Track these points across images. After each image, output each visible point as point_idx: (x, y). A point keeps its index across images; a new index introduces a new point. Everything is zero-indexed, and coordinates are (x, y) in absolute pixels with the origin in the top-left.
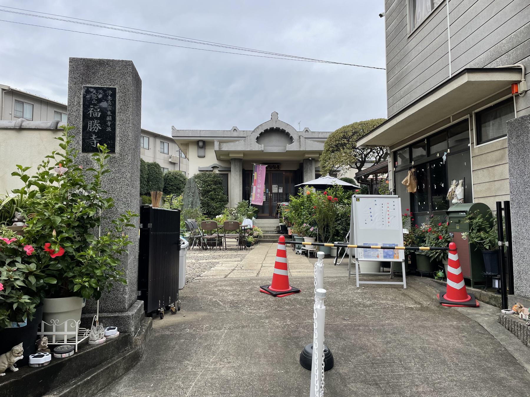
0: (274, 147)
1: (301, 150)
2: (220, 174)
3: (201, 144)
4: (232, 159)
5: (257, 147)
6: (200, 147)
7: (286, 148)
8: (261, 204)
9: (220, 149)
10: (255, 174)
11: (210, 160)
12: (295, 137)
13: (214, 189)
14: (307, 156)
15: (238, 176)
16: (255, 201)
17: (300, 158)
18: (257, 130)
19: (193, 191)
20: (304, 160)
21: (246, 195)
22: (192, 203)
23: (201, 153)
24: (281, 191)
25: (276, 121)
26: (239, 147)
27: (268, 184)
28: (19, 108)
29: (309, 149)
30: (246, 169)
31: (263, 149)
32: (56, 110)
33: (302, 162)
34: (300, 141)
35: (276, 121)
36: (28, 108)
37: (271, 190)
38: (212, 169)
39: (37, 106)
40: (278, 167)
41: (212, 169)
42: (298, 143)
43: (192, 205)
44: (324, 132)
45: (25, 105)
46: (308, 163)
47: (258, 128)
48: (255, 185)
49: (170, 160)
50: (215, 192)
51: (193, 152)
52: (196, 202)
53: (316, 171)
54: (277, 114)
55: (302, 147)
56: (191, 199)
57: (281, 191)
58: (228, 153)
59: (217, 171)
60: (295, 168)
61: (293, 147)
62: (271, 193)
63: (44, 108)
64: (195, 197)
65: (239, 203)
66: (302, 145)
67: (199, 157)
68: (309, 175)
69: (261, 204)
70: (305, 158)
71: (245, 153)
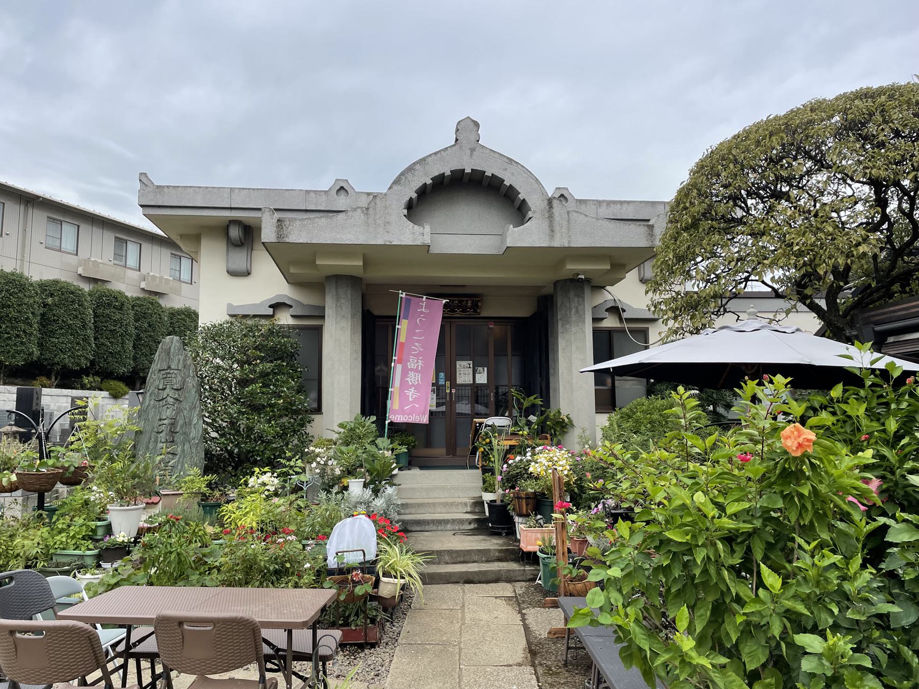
0: (466, 236)
1: (556, 244)
2: (294, 327)
3: (235, 232)
4: (328, 278)
5: (406, 234)
6: (235, 245)
7: (503, 241)
8: (425, 420)
9: (279, 236)
10: (403, 327)
11: (266, 286)
12: (535, 203)
13: (264, 375)
14: (572, 267)
15: (348, 332)
16: (403, 412)
17: (541, 278)
18: (409, 176)
19: (177, 381)
20: (556, 283)
21: (374, 395)
22: (173, 425)
23: (239, 259)
24: (482, 378)
25: (472, 150)
26: (350, 232)
27: (445, 362)
28: (53, 229)
29: (581, 241)
30: (376, 312)
31: (427, 240)
32: (50, 215)
33: (549, 290)
34: (551, 217)
35: (472, 150)
36: (69, 231)
37: (451, 376)
38: (270, 311)
39: (85, 228)
40: (475, 307)
41: (270, 311)
42: (545, 225)
43: (173, 433)
44: (615, 202)
45: (130, 245)
46: (572, 294)
47: (411, 169)
48: (400, 361)
49: (143, 285)
50: (265, 385)
51: (213, 261)
52: (187, 424)
53: (595, 320)
54: (477, 125)
55: (558, 235)
56: (168, 413)
57: (482, 378)
58: (314, 251)
59: (285, 319)
60: (523, 311)
61: (530, 235)
62: (454, 384)
63: (97, 231)
64: (186, 405)
65: (341, 426)
66: (557, 228)
67: (233, 273)
68: (574, 329)
69: (425, 420)
70: (562, 275)
71: (369, 254)
